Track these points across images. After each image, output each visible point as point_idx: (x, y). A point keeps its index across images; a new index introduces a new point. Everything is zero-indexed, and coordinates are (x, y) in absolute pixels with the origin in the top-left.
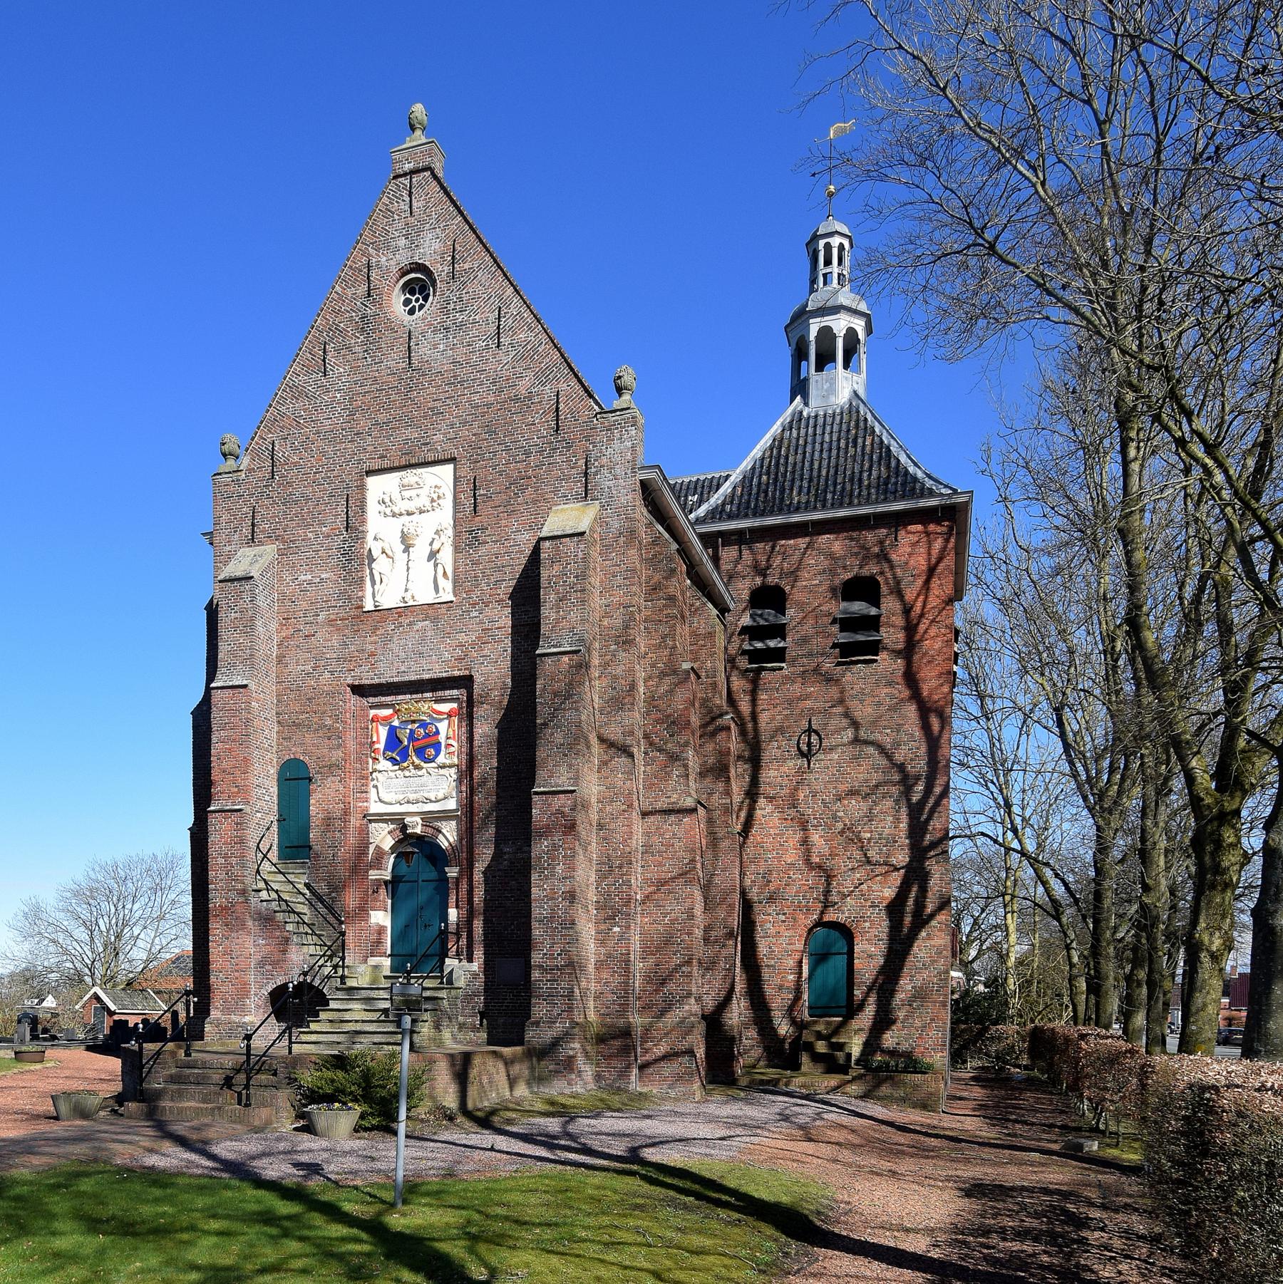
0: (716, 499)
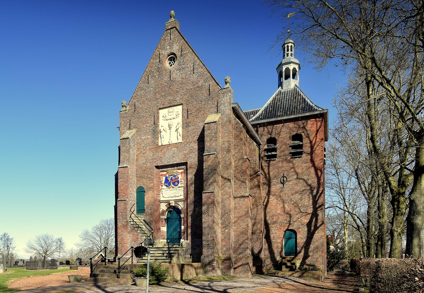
0: (258, 115)
